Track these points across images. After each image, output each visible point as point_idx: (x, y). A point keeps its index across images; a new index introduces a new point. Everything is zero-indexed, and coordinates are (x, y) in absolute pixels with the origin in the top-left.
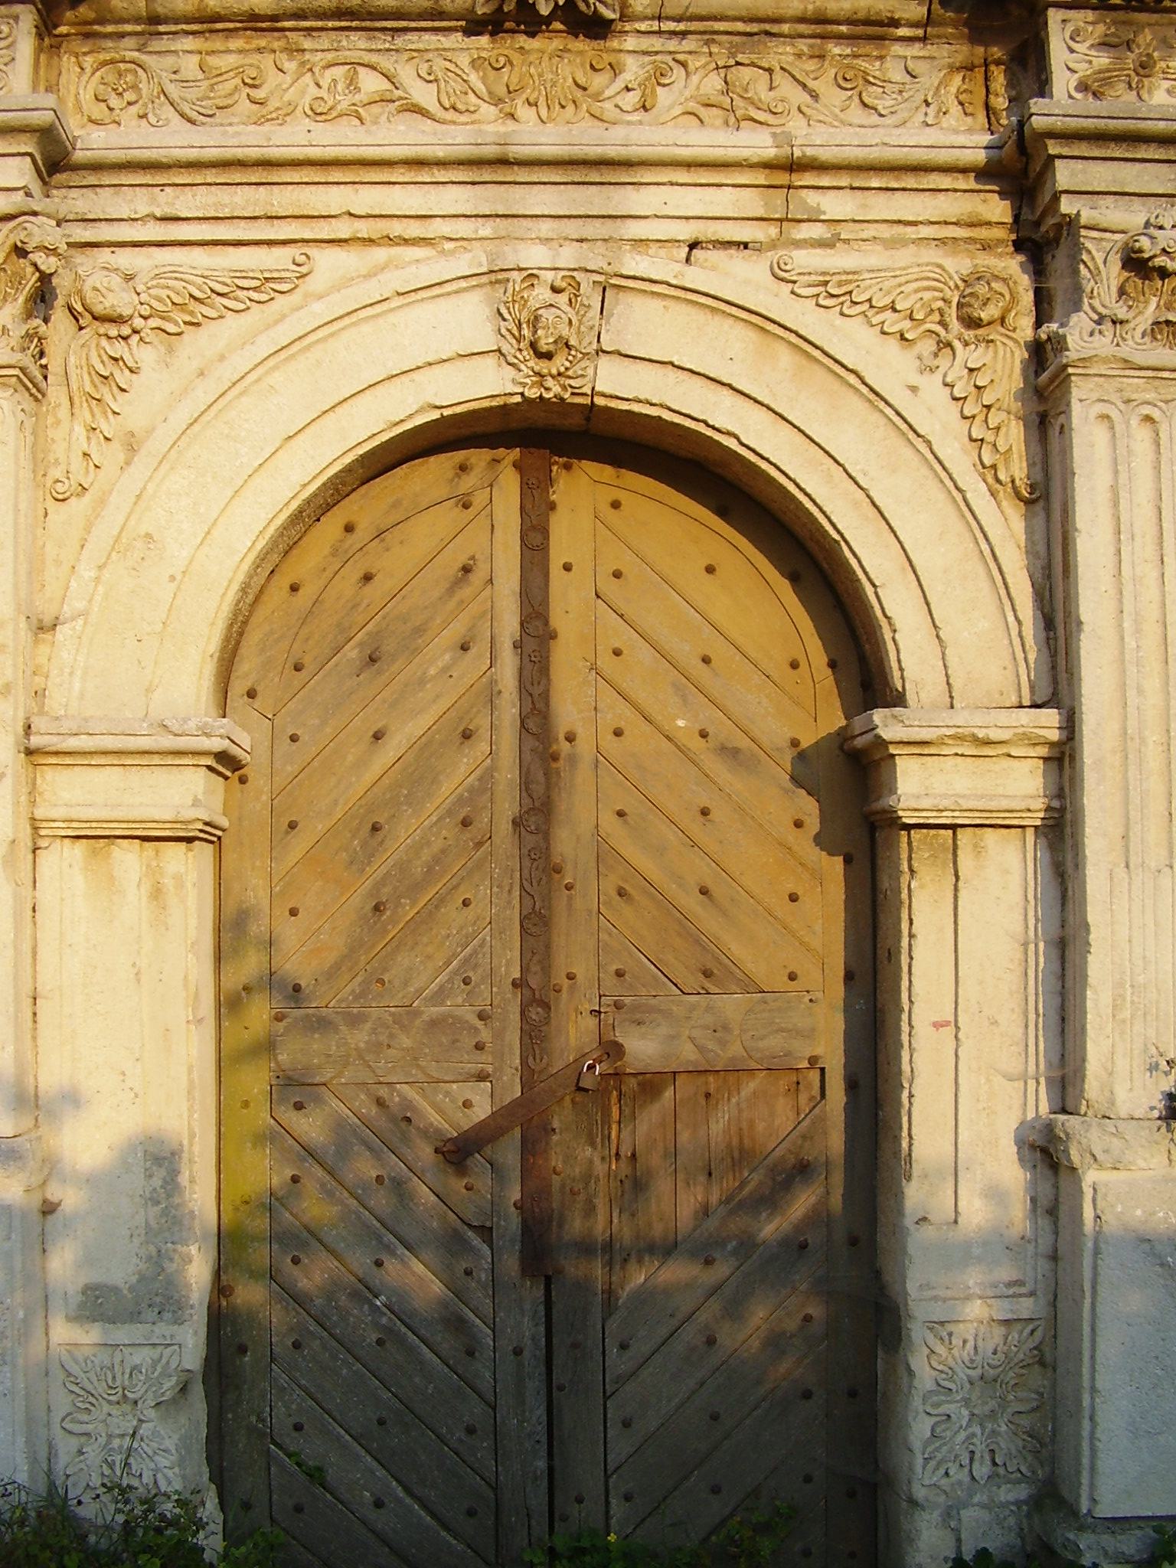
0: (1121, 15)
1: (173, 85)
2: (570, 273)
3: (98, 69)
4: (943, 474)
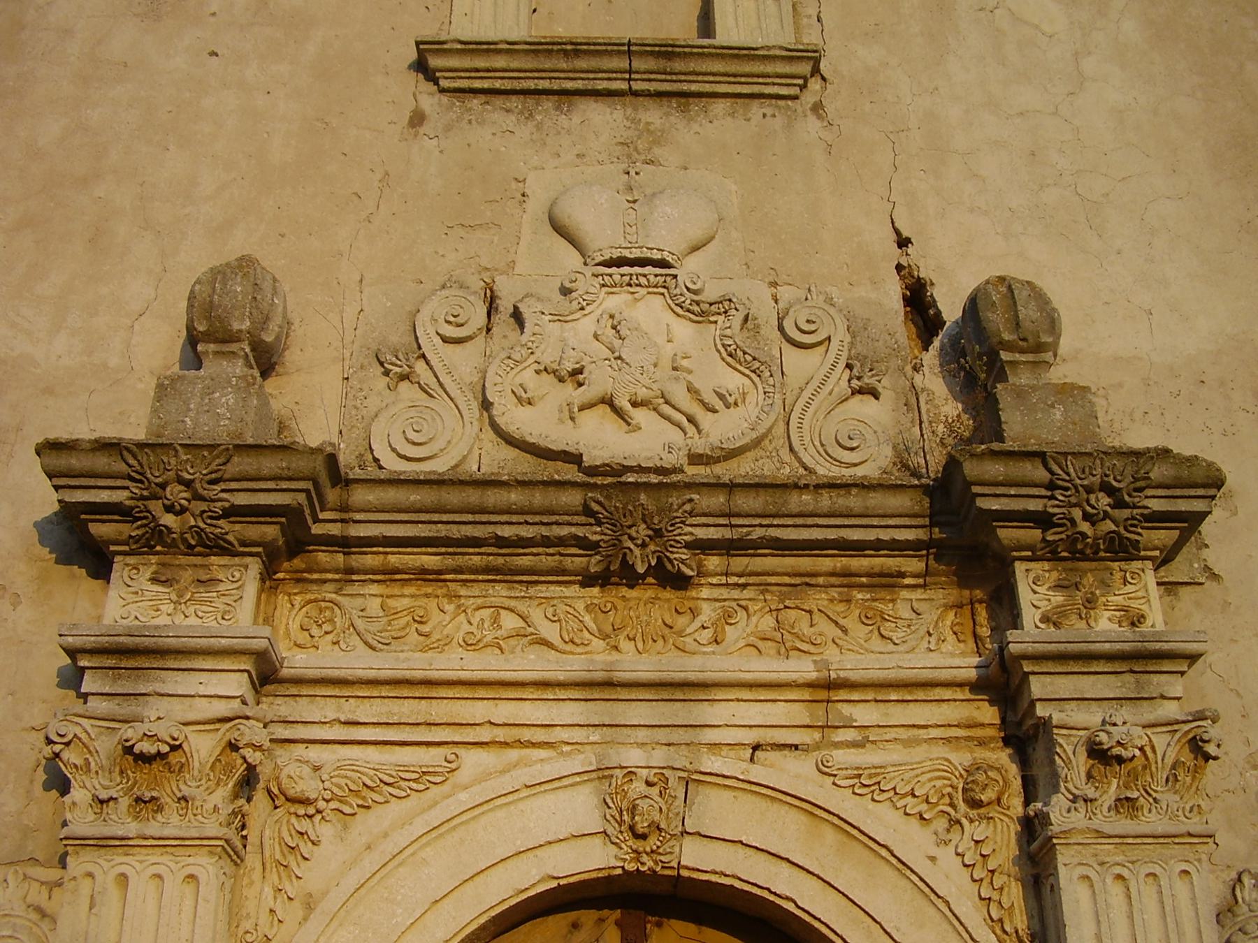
0: (1069, 564)
1: (360, 620)
2: (661, 771)
3: (304, 606)
4: (960, 928)
